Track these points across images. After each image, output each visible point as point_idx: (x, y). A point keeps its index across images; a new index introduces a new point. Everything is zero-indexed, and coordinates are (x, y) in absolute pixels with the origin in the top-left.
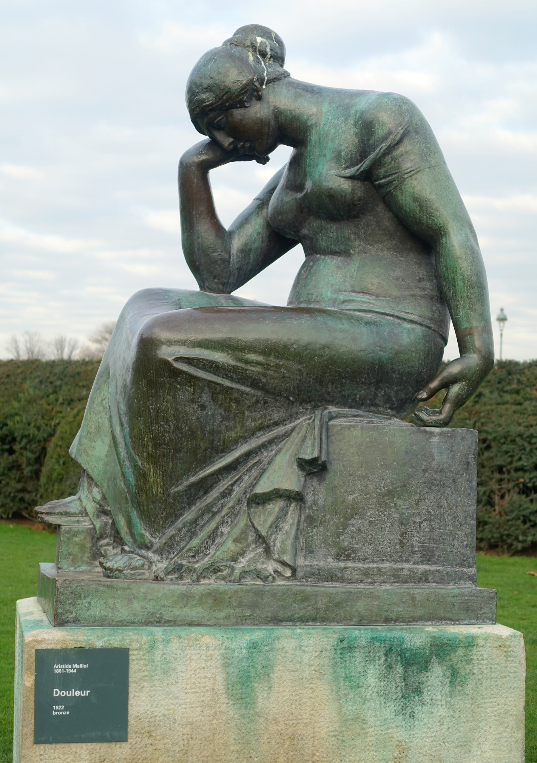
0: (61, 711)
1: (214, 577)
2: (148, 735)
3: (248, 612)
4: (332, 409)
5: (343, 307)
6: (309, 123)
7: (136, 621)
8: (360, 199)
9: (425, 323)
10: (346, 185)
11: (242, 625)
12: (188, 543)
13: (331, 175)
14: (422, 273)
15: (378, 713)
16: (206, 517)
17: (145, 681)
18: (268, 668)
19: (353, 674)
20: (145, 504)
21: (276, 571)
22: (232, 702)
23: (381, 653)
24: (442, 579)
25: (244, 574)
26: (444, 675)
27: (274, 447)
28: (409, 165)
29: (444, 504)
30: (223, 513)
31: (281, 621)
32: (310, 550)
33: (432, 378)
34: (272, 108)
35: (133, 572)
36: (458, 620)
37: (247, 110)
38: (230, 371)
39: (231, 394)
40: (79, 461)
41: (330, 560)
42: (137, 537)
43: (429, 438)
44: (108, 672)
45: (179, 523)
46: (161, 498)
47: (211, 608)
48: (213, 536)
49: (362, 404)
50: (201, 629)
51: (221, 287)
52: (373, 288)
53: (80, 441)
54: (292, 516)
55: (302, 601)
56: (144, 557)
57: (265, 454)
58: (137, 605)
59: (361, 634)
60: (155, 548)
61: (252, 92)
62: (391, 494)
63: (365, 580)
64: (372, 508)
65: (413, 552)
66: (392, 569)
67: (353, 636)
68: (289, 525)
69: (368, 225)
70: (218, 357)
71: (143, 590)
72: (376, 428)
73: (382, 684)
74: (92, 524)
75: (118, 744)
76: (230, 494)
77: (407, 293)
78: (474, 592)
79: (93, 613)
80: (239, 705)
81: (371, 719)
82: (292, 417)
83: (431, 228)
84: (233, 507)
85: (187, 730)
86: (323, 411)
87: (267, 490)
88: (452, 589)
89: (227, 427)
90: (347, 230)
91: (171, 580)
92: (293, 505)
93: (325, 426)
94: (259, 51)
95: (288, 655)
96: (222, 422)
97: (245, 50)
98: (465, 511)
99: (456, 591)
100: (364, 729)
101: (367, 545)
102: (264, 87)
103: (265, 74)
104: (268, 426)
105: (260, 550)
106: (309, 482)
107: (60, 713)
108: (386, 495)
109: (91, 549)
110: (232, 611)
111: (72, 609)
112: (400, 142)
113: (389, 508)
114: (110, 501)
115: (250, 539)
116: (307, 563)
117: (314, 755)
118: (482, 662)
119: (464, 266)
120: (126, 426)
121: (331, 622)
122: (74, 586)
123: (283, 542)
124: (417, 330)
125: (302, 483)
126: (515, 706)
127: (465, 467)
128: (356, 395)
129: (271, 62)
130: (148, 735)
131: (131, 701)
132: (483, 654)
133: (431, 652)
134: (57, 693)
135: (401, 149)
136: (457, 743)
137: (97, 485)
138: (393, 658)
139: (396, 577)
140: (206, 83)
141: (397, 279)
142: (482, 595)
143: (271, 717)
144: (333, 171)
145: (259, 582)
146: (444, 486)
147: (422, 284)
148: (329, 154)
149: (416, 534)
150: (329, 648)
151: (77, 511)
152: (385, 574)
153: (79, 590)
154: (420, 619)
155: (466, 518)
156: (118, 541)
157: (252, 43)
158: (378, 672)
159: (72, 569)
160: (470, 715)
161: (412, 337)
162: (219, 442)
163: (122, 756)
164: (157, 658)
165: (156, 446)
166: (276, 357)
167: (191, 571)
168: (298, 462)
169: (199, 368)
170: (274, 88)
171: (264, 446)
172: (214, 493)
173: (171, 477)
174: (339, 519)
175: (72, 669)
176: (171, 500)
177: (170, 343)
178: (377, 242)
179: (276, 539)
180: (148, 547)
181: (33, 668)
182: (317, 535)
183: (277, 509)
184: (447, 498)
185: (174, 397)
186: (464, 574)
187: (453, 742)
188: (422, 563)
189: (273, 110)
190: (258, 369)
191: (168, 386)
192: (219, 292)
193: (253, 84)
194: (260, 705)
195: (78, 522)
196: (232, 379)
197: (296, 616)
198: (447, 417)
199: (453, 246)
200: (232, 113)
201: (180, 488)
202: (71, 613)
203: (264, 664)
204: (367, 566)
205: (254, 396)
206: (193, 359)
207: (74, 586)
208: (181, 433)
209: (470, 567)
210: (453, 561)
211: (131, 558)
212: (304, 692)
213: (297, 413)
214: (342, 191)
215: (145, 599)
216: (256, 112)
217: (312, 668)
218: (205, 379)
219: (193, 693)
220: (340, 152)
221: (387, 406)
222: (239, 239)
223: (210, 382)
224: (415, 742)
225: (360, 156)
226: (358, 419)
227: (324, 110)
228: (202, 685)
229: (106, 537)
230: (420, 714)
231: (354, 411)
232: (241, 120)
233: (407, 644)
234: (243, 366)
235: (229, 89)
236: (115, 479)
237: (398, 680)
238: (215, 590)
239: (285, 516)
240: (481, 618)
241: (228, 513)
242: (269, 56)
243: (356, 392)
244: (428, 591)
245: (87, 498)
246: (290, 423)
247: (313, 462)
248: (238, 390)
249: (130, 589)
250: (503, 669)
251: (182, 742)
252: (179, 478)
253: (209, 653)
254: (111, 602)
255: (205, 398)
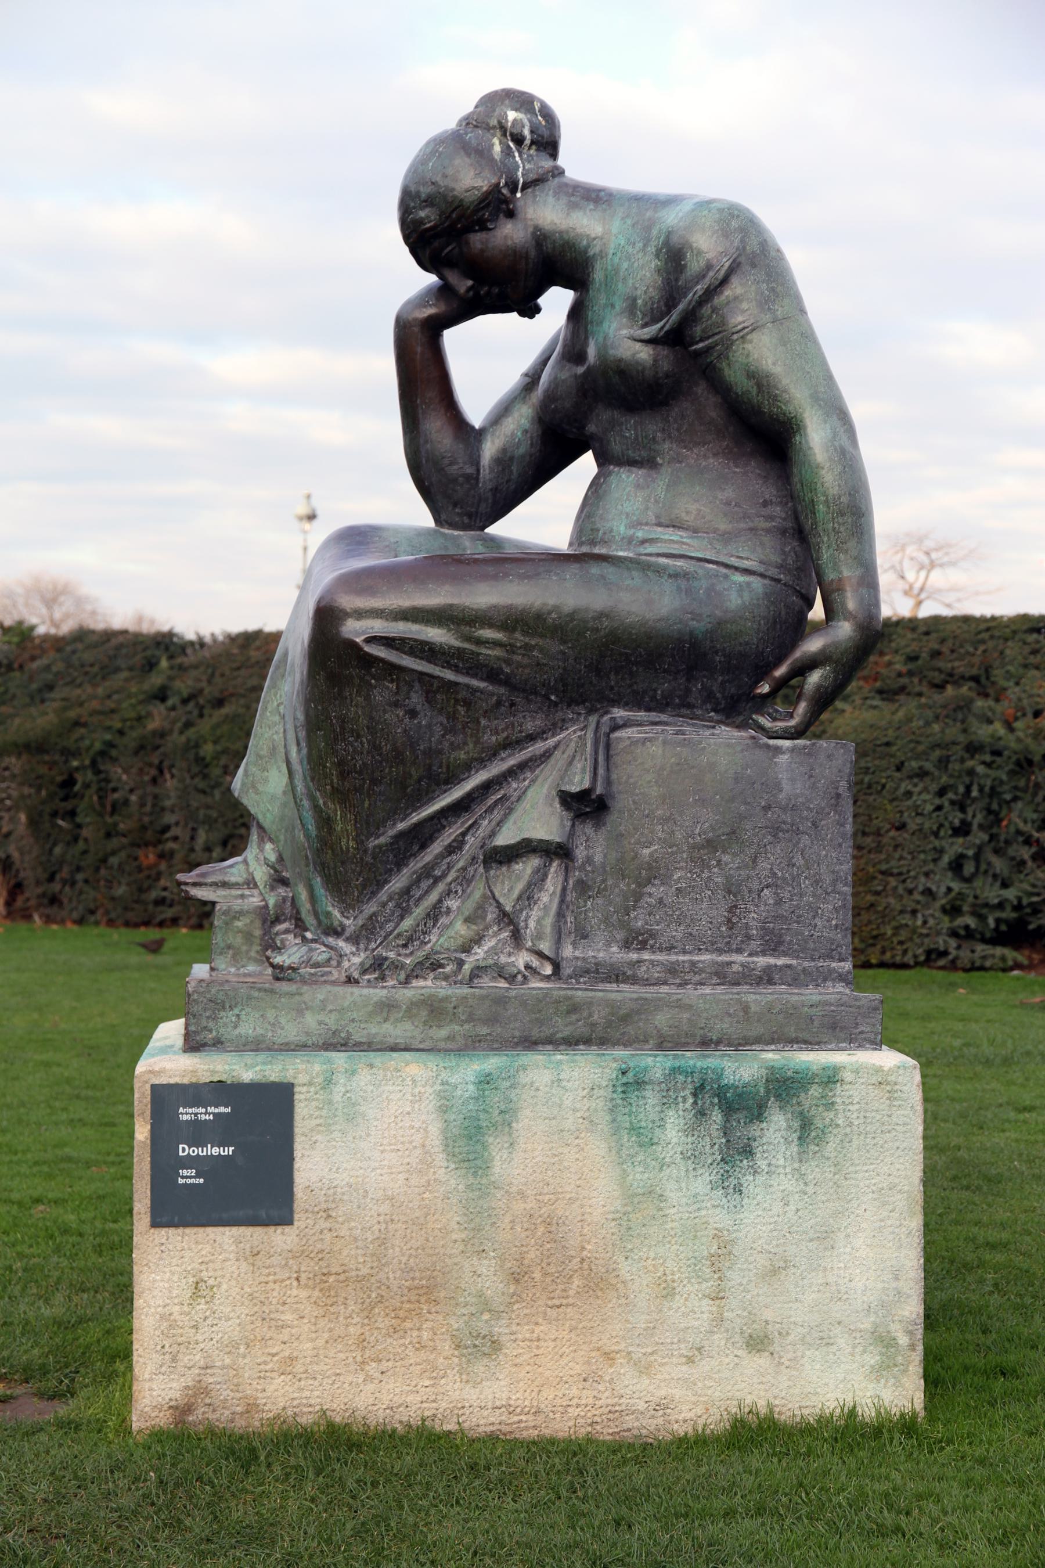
0: (191, 1177)
1: (432, 975)
2: (325, 1215)
3: (484, 1030)
4: (619, 713)
5: (642, 550)
6: (591, 253)
7: (310, 1043)
8: (667, 376)
9: (769, 573)
10: (644, 354)
11: (475, 1049)
12: (397, 925)
13: (624, 339)
14: (769, 492)
15: (683, 1185)
16: (425, 884)
17: (319, 1132)
18: (508, 1115)
19: (643, 1124)
20: (332, 865)
21: (528, 967)
22: (453, 1166)
23: (687, 1092)
24: (796, 979)
25: (478, 971)
26: (789, 1127)
27: (528, 774)
28: (740, 319)
29: (799, 860)
30: (449, 879)
31: (536, 1043)
32: (582, 935)
33: (777, 664)
34: (531, 230)
35: (313, 971)
36: (818, 1043)
37: (491, 233)
38: (453, 656)
39: (457, 693)
40: (245, 801)
41: (615, 949)
42: (322, 918)
43: (774, 756)
44: (262, 1120)
45: (383, 896)
46: (355, 856)
47: (425, 1023)
48: (435, 914)
49: (667, 705)
50: (407, 1055)
51: (466, 520)
52: (689, 519)
53: (246, 771)
54: (553, 883)
55: (569, 1012)
56: (331, 948)
57: (514, 785)
58: (311, 1020)
59: (656, 1064)
60: (347, 934)
61: (498, 204)
62: (711, 845)
63: (671, 981)
64: (681, 868)
65: (749, 937)
66: (714, 963)
67: (643, 1064)
68: (548, 895)
69: (683, 417)
70: (435, 634)
71: (320, 997)
72: (684, 743)
73: (690, 1139)
74: (264, 900)
75: (280, 1229)
76: (460, 848)
77: (742, 525)
78: (845, 998)
79: (243, 1032)
80: (464, 1171)
81: (672, 1195)
82: (556, 727)
83: (778, 420)
84: (464, 869)
85: (385, 1208)
86: (602, 716)
87: (512, 842)
88: (811, 994)
89: (452, 744)
90: (652, 426)
91: (369, 981)
92: (555, 864)
93: (602, 740)
94: (512, 135)
95: (540, 1094)
96: (443, 736)
97: (488, 135)
98: (833, 872)
99: (816, 998)
100: (661, 1209)
101: (673, 926)
102: (519, 195)
103: (520, 174)
104: (518, 742)
105: (505, 934)
106: (579, 827)
107: (189, 1181)
108: (703, 847)
109: (262, 939)
110: (457, 1028)
111: (211, 1024)
112: (724, 281)
113: (709, 867)
114: (288, 864)
115: (490, 917)
116: (577, 954)
117: (583, 1248)
118: (850, 1107)
119: (830, 481)
120: (303, 744)
121: (614, 1045)
122: (213, 991)
123: (538, 922)
124: (754, 585)
125: (568, 829)
126: (906, 1177)
127: (833, 801)
128: (655, 690)
129: (532, 152)
130: (325, 1215)
131: (298, 1164)
132: (853, 1095)
133: (768, 1091)
134: (184, 1150)
135: (728, 293)
136: (811, 1235)
137: (271, 840)
138: (707, 1099)
139: (721, 975)
140: (425, 191)
141: (728, 503)
142: (858, 1003)
143: (514, 1189)
144: (624, 332)
145: (503, 984)
146: (798, 832)
147: (768, 510)
148: (619, 305)
149: (752, 908)
150: (604, 1084)
151: (240, 880)
152: (702, 971)
153: (221, 996)
154: (758, 1040)
155: (834, 882)
156: (300, 926)
157: (500, 122)
158: (682, 1122)
159: (233, 970)
160: (832, 1191)
161: (746, 596)
162: (441, 767)
163: (286, 1247)
164: (337, 1097)
165: (343, 775)
166: (525, 633)
167: (397, 967)
168: (560, 797)
169: (405, 653)
170: (535, 196)
171: (511, 773)
172: (436, 848)
173: (368, 823)
174: (628, 885)
175: (205, 1114)
176: (368, 859)
177: (360, 614)
178: (697, 444)
179: (528, 917)
180: (336, 932)
181: (148, 1113)
182: (594, 909)
183: (529, 871)
184: (803, 851)
185: (367, 698)
186: (831, 971)
187: (806, 1233)
188: (764, 953)
189: (534, 233)
190: (497, 652)
191: (357, 681)
192: (465, 527)
193: (500, 192)
194: (497, 1170)
195: (242, 896)
196: (457, 669)
197: (560, 1035)
198: (801, 723)
199: (810, 448)
200: (473, 238)
201: (382, 840)
202: (211, 1031)
203: (503, 1108)
204: (673, 958)
205: (493, 694)
206: (393, 639)
207: (213, 991)
208: (380, 755)
209: (841, 960)
210: (815, 950)
211: (311, 950)
212: (566, 1150)
213: (563, 720)
214: (637, 363)
215: (323, 1010)
216: (506, 237)
217: (579, 1115)
218: (413, 670)
219: (392, 1151)
220: (635, 300)
221: (709, 706)
222: (493, 442)
223: (422, 674)
224: (744, 1232)
225: (667, 305)
226: (659, 728)
227: (614, 231)
228: (406, 1139)
229: (285, 921)
230: (751, 1187)
231: (654, 716)
232: (482, 251)
233: (729, 1078)
234: (473, 647)
235: (461, 200)
236: (294, 828)
237: (715, 1134)
238: (431, 996)
239: (543, 880)
240: (856, 1040)
241: (458, 878)
242: (528, 142)
243: (655, 685)
244: (770, 998)
245: (257, 859)
246: (553, 736)
247: (583, 795)
248: (467, 686)
249: (301, 994)
250: (886, 1118)
251: (377, 1227)
252: (381, 824)
253: (417, 1090)
254: (271, 1014)
255: (416, 699)
